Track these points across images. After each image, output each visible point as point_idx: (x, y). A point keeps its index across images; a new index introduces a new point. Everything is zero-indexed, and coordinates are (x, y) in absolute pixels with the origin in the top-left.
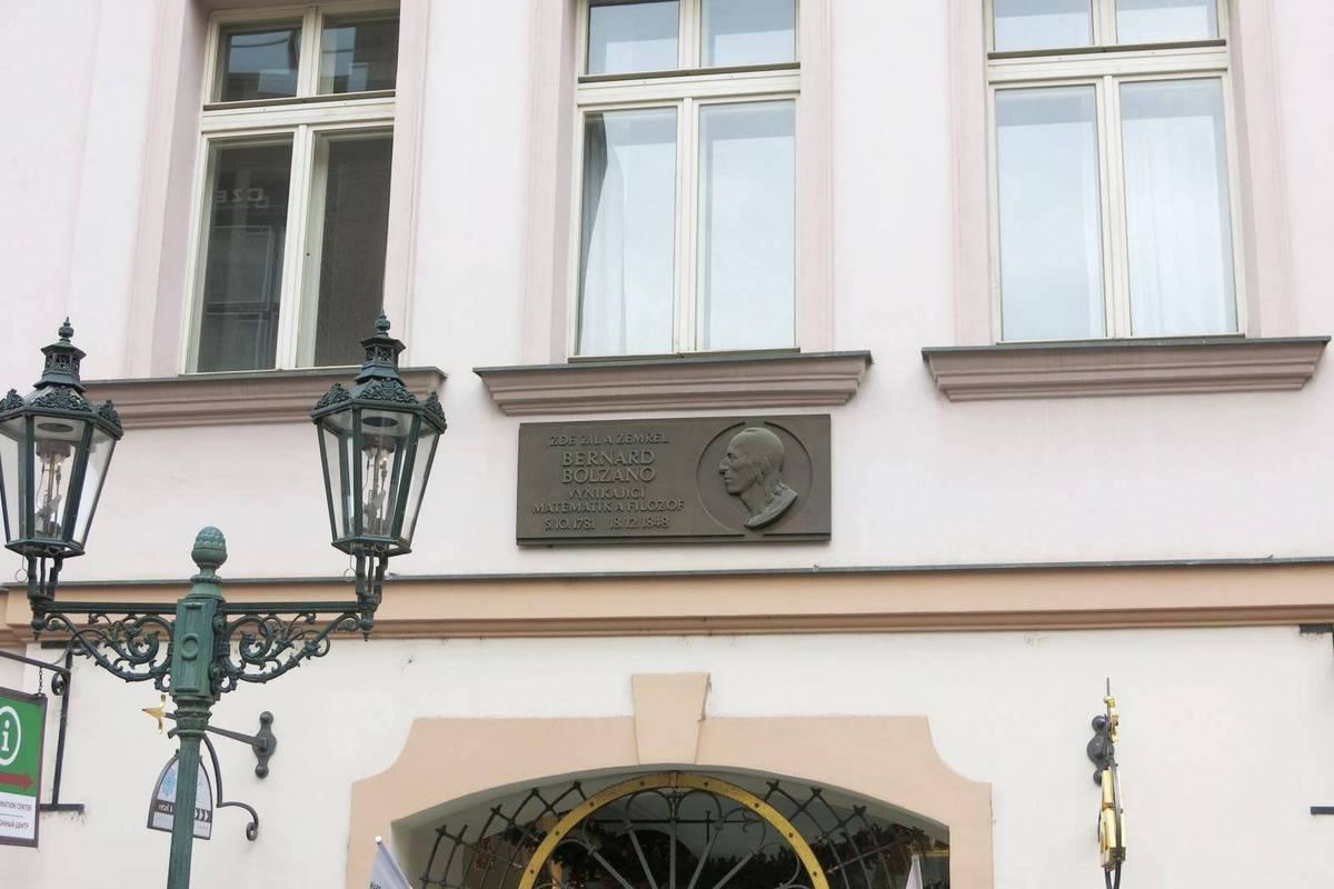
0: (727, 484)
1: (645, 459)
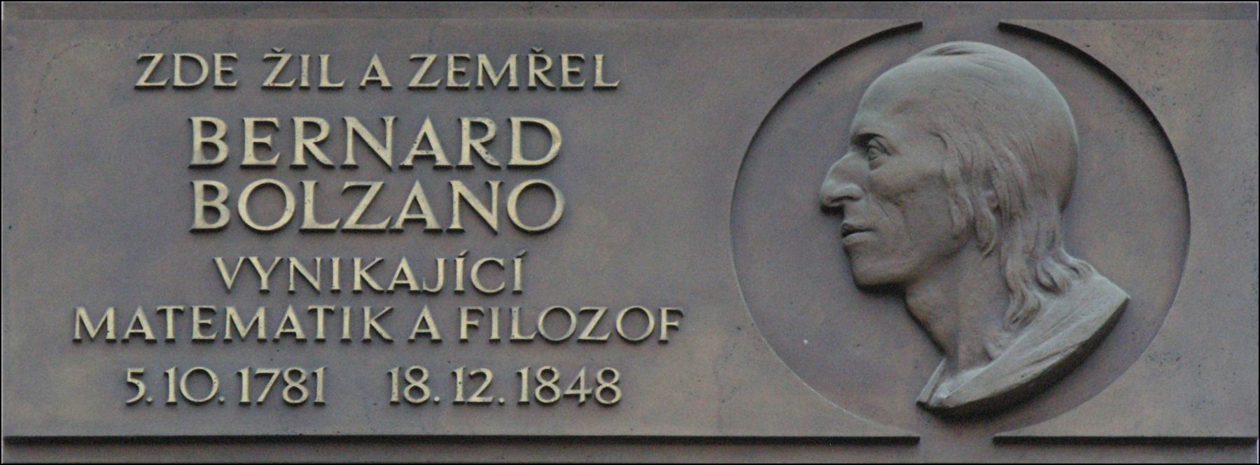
0: (848, 252)
1: (184, 77)
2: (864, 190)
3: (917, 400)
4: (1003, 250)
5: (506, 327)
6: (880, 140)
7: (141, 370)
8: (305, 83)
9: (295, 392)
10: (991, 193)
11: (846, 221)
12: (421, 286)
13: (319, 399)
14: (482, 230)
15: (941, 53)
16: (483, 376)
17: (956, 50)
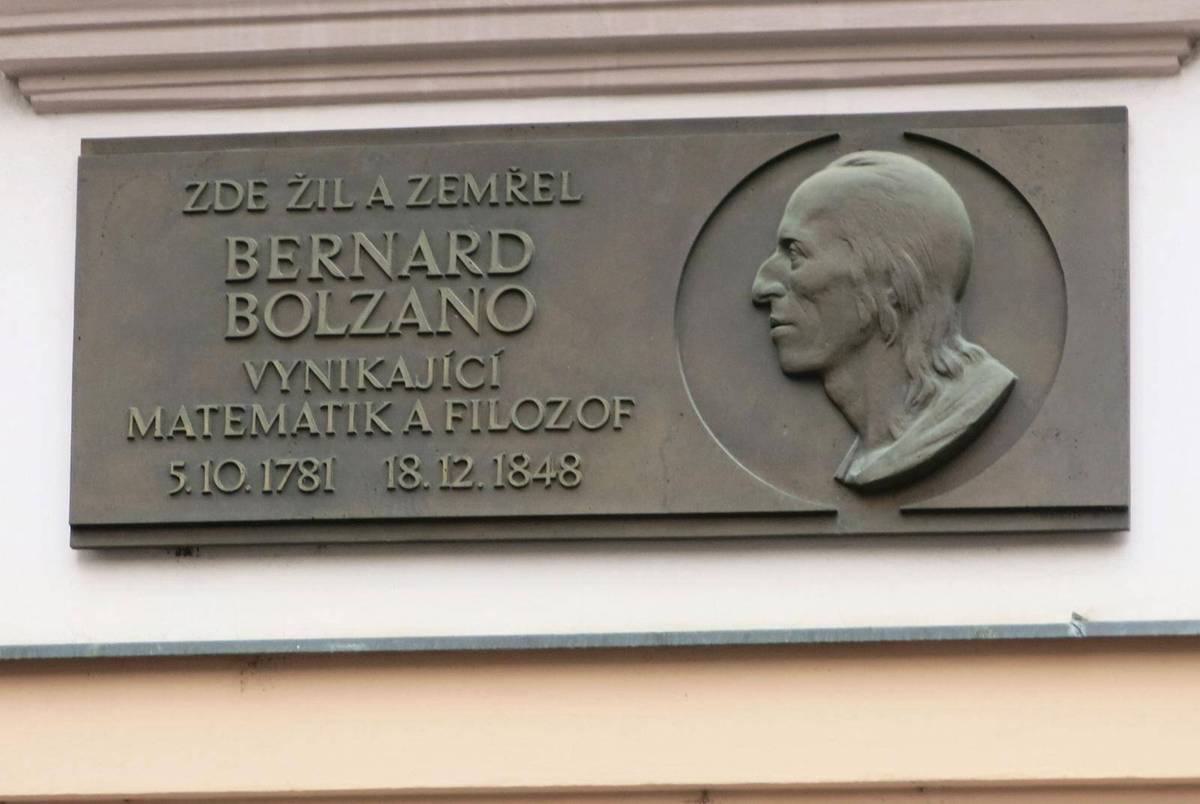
0: (776, 342)
2: (787, 288)
3: (835, 475)
4: (904, 340)
5: (484, 420)
6: (799, 245)
7: (181, 464)
8: (321, 204)
9: (309, 480)
10: (890, 291)
11: (772, 315)
12: (414, 383)
13: (329, 486)
14: (466, 330)
15: (851, 163)
16: (463, 463)
17: (862, 162)
